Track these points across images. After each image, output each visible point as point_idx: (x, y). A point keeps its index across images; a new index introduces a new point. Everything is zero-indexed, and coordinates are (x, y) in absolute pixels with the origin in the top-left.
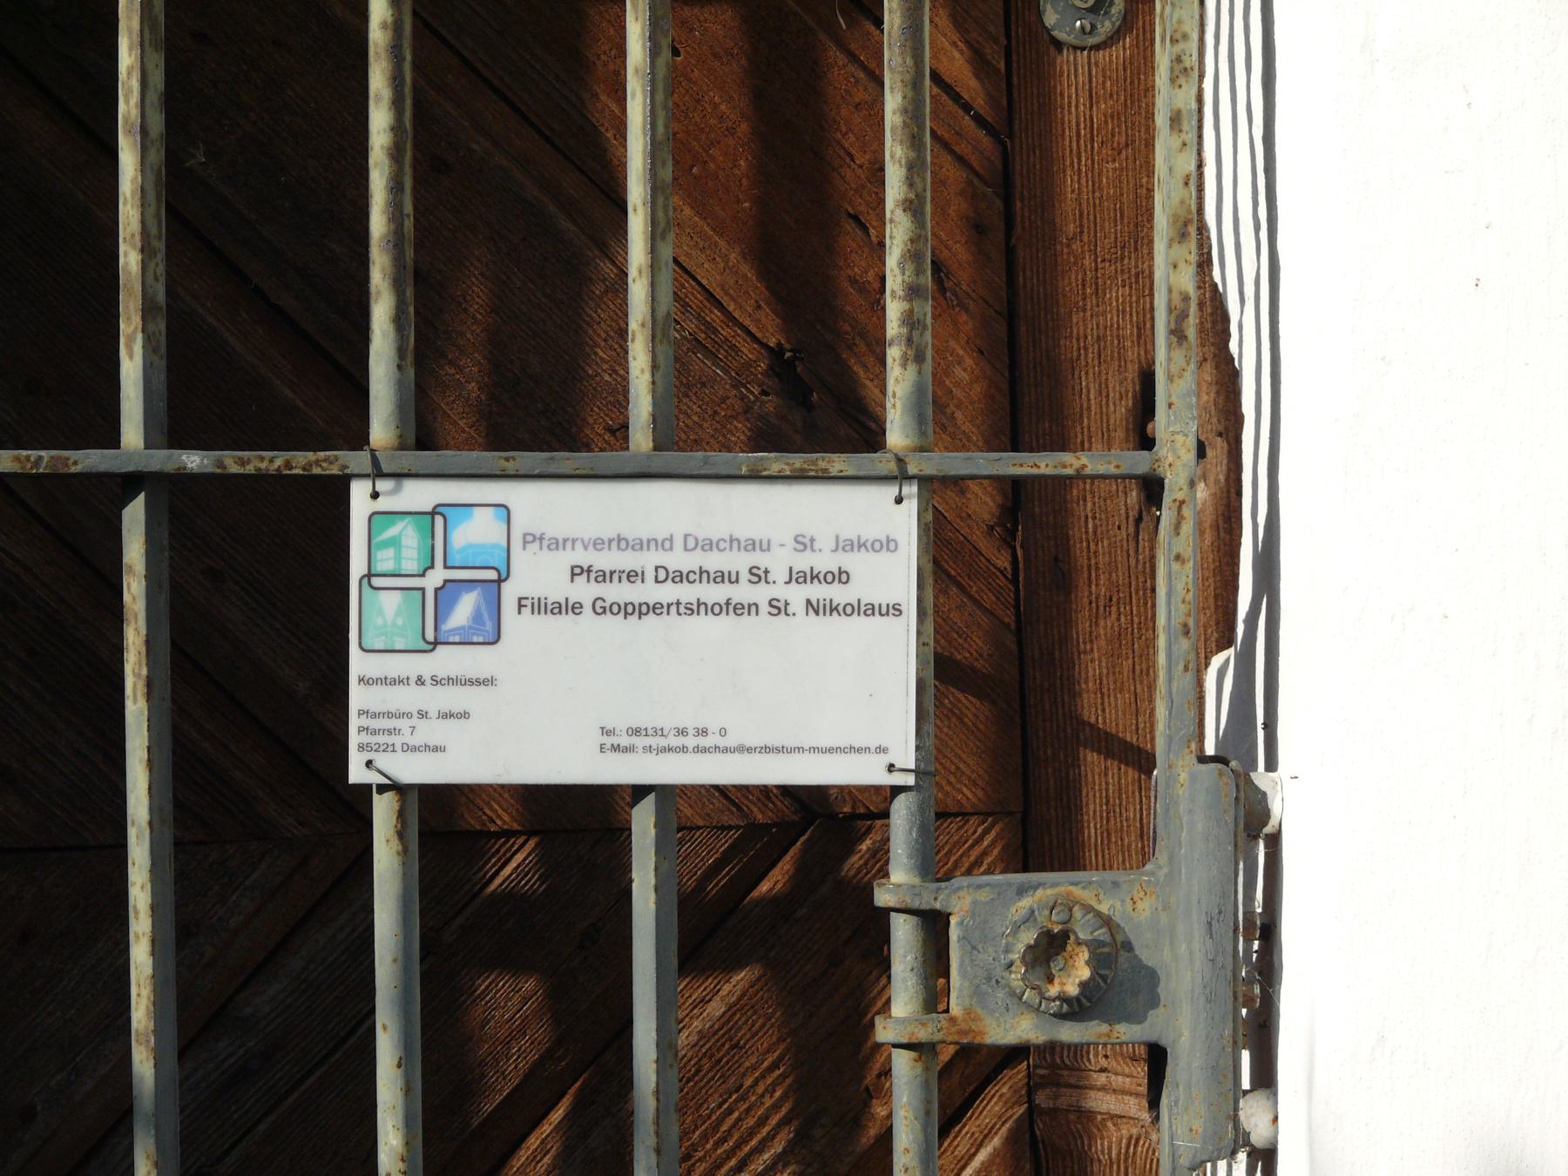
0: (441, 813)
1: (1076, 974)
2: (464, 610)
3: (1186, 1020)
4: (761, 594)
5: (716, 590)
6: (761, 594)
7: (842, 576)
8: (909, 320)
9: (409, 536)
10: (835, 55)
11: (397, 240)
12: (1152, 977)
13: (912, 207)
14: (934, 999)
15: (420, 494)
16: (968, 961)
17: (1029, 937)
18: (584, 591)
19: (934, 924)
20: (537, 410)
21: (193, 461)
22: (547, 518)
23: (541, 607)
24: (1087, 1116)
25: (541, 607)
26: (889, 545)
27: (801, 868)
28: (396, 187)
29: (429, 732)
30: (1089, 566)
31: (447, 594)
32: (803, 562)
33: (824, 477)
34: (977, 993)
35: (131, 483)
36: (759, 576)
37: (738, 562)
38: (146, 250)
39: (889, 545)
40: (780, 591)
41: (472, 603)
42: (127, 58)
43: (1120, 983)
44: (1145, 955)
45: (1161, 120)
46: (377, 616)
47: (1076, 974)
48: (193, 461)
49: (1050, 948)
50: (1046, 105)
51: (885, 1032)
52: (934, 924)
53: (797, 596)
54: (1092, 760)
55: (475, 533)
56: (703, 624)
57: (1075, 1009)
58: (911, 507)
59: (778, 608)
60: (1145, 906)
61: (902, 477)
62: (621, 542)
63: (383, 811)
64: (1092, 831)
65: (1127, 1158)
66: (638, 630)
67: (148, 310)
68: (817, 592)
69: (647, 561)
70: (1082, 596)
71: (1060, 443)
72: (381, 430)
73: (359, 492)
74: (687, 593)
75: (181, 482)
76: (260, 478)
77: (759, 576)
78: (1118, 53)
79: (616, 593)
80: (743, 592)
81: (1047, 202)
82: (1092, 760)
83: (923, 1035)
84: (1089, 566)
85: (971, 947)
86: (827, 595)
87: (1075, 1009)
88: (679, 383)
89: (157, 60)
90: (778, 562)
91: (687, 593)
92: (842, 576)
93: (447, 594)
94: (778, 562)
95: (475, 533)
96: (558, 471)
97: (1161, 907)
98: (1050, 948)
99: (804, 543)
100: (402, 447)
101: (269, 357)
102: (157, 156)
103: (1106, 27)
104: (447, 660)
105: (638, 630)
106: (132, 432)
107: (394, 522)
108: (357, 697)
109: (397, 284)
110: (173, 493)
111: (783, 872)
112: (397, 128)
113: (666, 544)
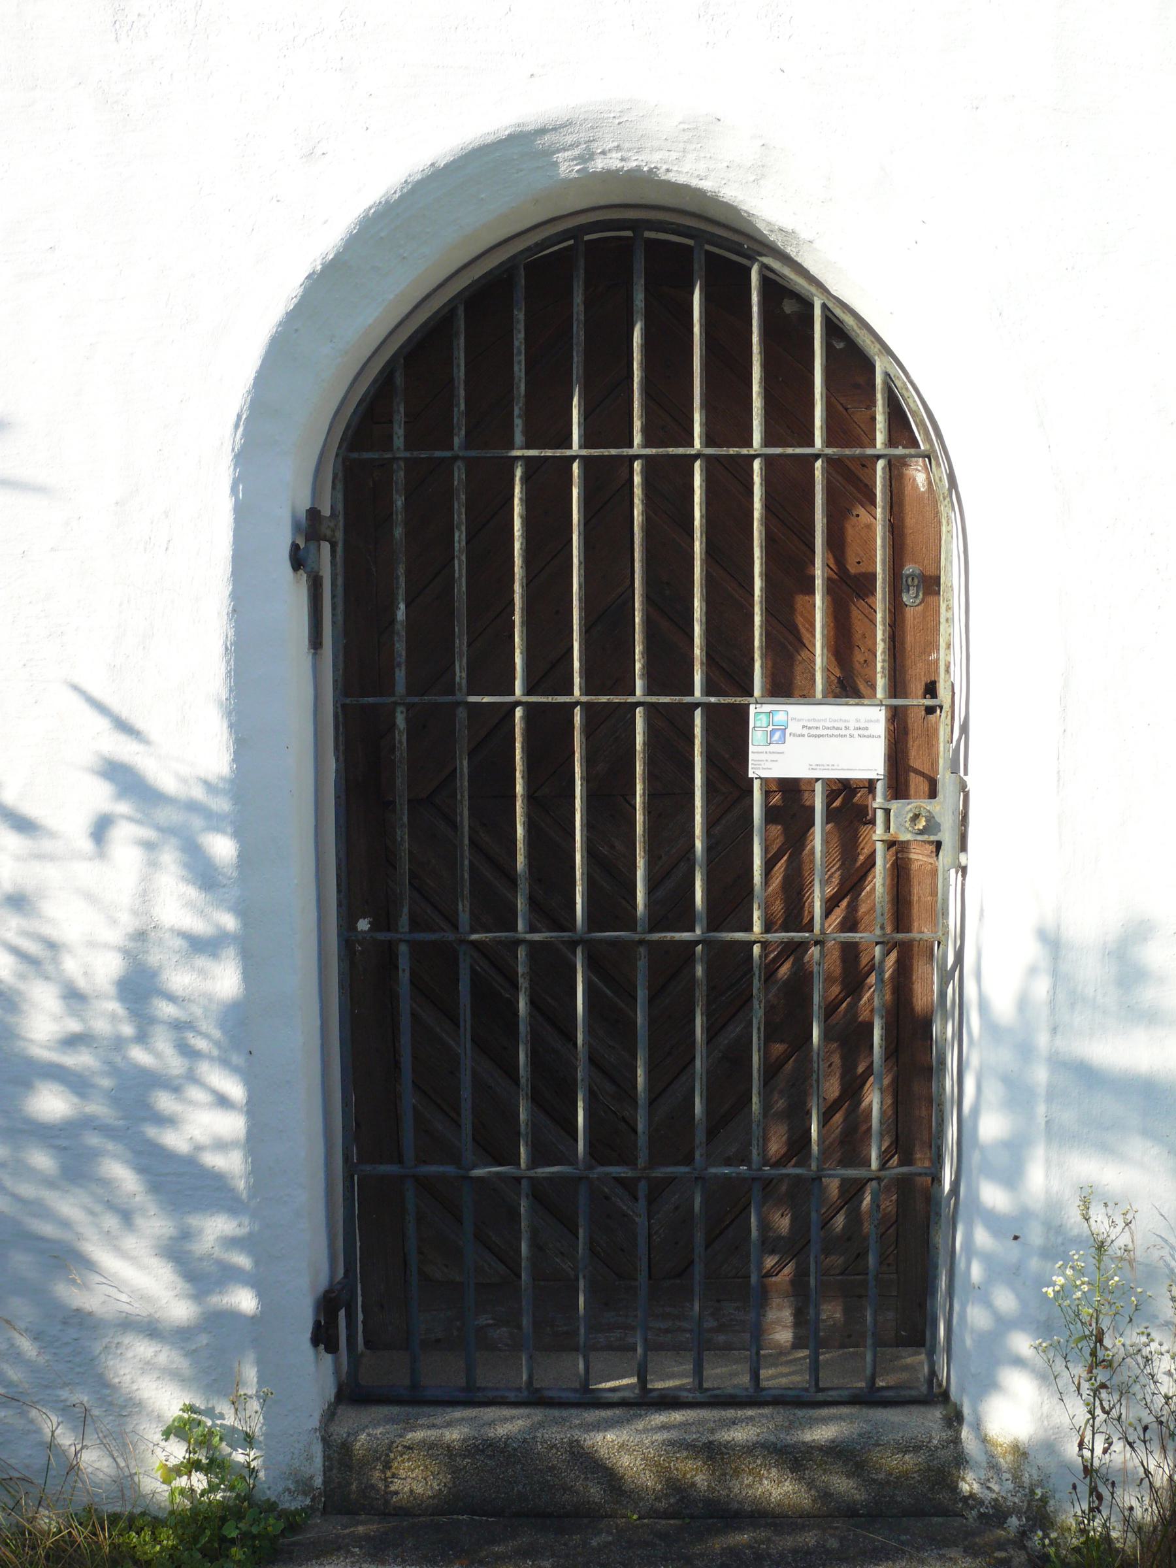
0: (765, 781)
1: (922, 824)
2: (777, 736)
3: (947, 837)
4: (847, 732)
5: (837, 732)
6: (847, 732)
7: (867, 729)
8: (883, 668)
9: (764, 718)
10: (853, 607)
11: (761, 648)
12: (939, 825)
13: (883, 640)
14: (887, 828)
15: (767, 708)
16: (891, 822)
17: (911, 815)
18: (805, 731)
19: (887, 812)
20: (783, 688)
21: (713, 700)
22: (794, 714)
23: (795, 735)
24: (909, 859)
25: (795, 735)
26: (878, 721)
27: (844, 799)
28: (761, 635)
29: (768, 765)
30: (549, 728)
31: (773, 732)
32: (857, 725)
33: (863, 705)
34: (898, 828)
35: (697, 705)
36: (847, 728)
37: (842, 725)
38: (701, 649)
39: (878, 721)
40: (852, 732)
41: (779, 734)
42: (697, 603)
43: (932, 826)
44: (937, 819)
45: (942, 620)
46: (756, 738)
47: (922, 824)
48: (713, 700)
49: (916, 817)
50: (903, 621)
51: (875, 838)
52: (887, 812)
53: (856, 733)
54: (912, 775)
55: (780, 718)
56: (834, 739)
57: (921, 832)
58: (883, 712)
59: (851, 736)
60: (938, 808)
61: (882, 705)
62: (814, 720)
63: (757, 785)
64: (912, 792)
65: (919, 870)
66: (811, 741)
67: (702, 664)
68: (861, 732)
69: (820, 725)
70: (910, 736)
71: (905, 696)
72: (757, 692)
73: (752, 707)
74: (830, 732)
75: (652, 704)
76: (729, 704)
77: (847, 728)
78: (921, 608)
79: (813, 732)
80: (843, 732)
81: (903, 643)
82: (912, 775)
83: (884, 838)
84: (549, 728)
85: (896, 816)
86: (863, 732)
87: (921, 832)
88: (827, 682)
89: (704, 604)
90: (851, 725)
91: (830, 732)
92: (867, 729)
93: (773, 732)
94: (851, 725)
95: (780, 718)
96: (950, 701)
97: (943, 809)
98: (916, 817)
99: (858, 721)
100: (763, 696)
101: (730, 674)
102: (704, 627)
103: (918, 601)
104: (772, 748)
105: (811, 741)
106: (698, 692)
107: (764, 716)
108: (751, 756)
109: (761, 658)
110: (707, 707)
111: (848, 798)
112: (761, 621)
113: (825, 720)
